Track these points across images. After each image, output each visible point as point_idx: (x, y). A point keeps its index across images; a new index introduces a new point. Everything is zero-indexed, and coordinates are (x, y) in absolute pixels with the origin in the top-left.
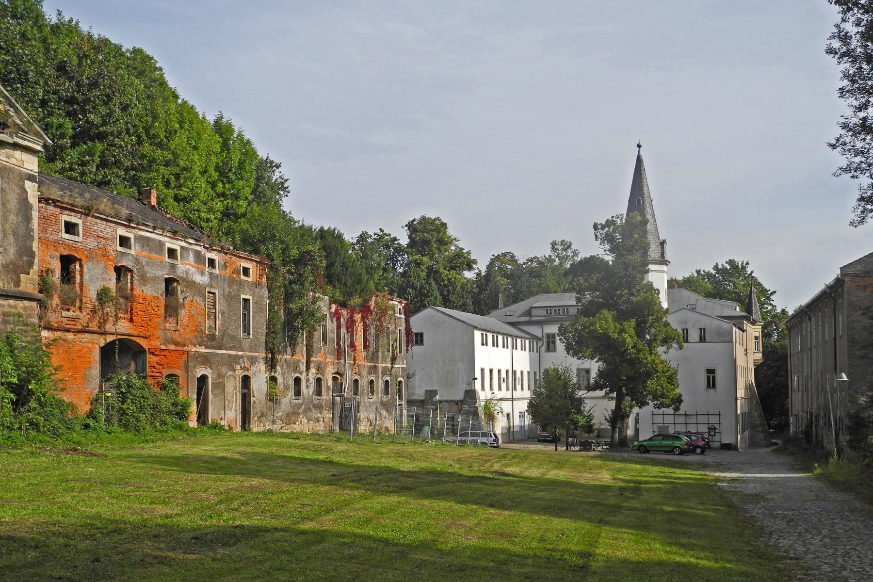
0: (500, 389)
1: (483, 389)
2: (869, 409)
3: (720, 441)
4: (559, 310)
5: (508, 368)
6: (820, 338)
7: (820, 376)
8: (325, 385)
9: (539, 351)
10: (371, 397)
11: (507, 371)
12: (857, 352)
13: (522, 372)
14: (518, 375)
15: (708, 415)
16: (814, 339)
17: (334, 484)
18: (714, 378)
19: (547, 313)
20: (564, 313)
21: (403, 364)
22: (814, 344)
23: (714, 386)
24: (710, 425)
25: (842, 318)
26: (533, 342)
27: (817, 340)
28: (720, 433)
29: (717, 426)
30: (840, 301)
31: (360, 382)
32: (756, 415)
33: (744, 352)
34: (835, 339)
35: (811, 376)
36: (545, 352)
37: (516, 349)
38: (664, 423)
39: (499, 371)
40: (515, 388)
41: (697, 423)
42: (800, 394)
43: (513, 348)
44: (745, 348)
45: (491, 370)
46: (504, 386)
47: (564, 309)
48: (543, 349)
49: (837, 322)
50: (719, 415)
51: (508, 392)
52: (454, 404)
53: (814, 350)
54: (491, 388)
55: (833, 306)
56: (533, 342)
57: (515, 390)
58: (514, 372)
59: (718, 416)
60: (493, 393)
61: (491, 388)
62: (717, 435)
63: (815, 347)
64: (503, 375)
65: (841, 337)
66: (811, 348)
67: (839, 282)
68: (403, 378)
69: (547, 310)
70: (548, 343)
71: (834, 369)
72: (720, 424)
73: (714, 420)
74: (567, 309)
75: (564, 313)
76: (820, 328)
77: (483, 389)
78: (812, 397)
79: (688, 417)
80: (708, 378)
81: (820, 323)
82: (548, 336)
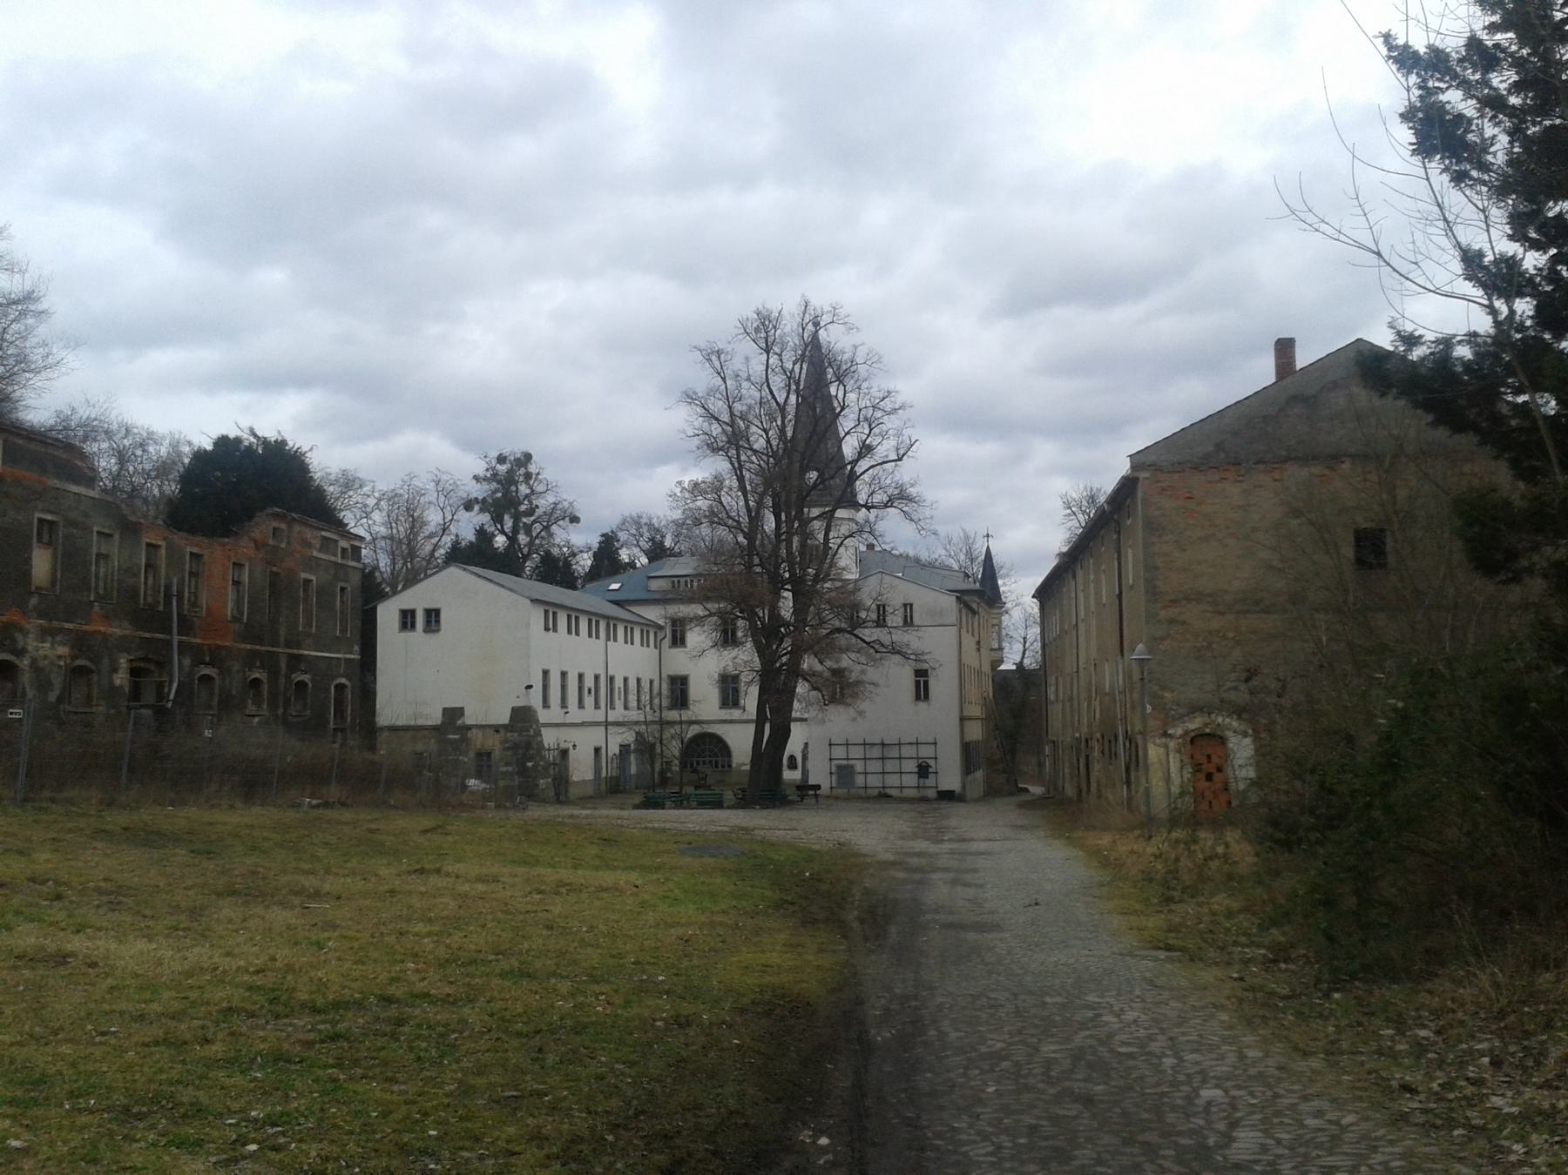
0: (581, 705)
1: (546, 704)
2: (1186, 718)
3: (937, 787)
4: (692, 581)
5: (597, 672)
6: (1092, 602)
7: (1092, 668)
11: (597, 677)
12: (1163, 613)
13: (626, 680)
14: (619, 683)
15: (917, 744)
16: (1082, 608)
18: (926, 683)
19: (673, 587)
20: (686, 585)
21: (351, 653)
22: (1082, 614)
23: (927, 697)
24: (920, 761)
25: (1134, 556)
26: (648, 632)
27: (1086, 608)
28: (936, 773)
29: (932, 762)
30: (1129, 522)
31: (217, 682)
32: (995, 746)
33: (974, 646)
34: (1120, 596)
35: (1077, 672)
36: (670, 647)
37: (615, 640)
38: (848, 759)
39: (581, 676)
41: (900, 758)
42: (1060, 706)
44: (977, 639)
45: (564, 674)
46: (589, 701)
47: (686, 582)
48: (667, 642)
49: (1123, 559)
50: (935, 744)
51: (598, 711)
52: (492, 732)
53: (1082, 628)
54: (564, 704)
55: (1115, 537)
56: (648, 632)
57: (613, 708)
60: (567, 713)
61: (564, 704)
62: (932, 778)
63: (1083, 620)
65: (1132, 588)
66: (1077, 624)
67: (1127, 487)
68: (347, 677)
70: (674, 633)
71: (1118, 652)
72: (936, 758)
73: (926, 752)
75: (686, 585)
76: (1092, 585)
77: (546, 704)
78: (1079, 703)
79: (886, 749)
80: (917, 683)
81: (1092, 577)
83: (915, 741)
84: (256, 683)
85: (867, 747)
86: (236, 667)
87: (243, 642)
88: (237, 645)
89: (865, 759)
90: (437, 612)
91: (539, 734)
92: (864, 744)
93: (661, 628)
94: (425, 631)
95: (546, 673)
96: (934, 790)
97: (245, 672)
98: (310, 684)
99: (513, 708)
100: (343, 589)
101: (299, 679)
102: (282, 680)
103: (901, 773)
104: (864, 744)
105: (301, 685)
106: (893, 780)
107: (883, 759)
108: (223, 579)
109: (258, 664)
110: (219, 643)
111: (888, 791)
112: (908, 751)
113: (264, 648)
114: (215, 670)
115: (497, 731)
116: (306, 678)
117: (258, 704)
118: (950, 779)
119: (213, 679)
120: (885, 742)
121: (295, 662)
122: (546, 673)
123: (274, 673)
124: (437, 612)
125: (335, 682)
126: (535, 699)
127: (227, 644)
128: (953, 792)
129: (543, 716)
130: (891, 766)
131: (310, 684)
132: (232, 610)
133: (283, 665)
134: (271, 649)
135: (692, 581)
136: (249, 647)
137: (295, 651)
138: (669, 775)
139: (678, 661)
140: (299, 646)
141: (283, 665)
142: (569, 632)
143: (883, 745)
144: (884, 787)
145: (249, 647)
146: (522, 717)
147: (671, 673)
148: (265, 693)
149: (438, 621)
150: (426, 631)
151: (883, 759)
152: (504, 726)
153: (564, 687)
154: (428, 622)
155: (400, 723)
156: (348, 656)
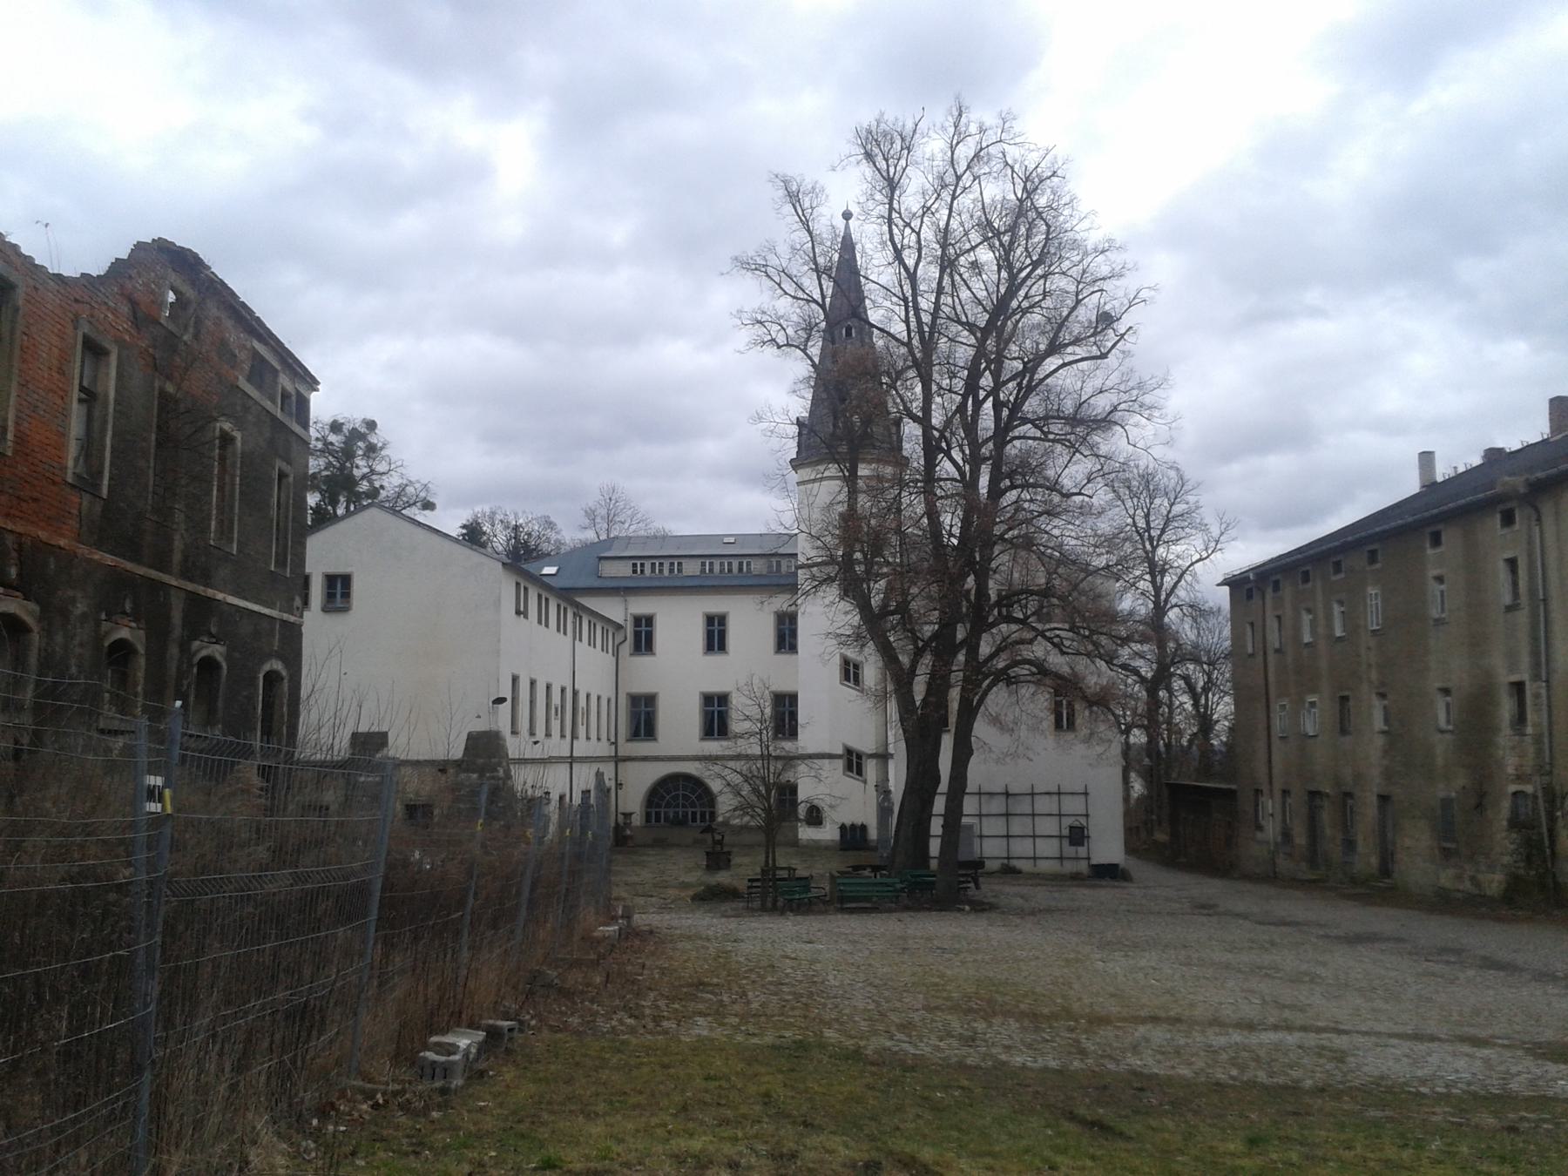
3: (1089, 859)
4: (661, 564)
5: (564, 685)
8: (1066, 633)
9: (616, 654)
10: (116, 725)
11: (563, 690)
13: (588, 696)
14: (582, 702)
15: (1059, 794)
17: (1536, 1043)
19: (635, 572)
31: (36, 637)
36: (631, 655)
37: (581, 640)
40: (574, 736)
43: (574, 639)
48: (627, 647)
50: (1086, 794)
58: (575, 693)
59: (1036, 797)
64: (556, 699)
69: (703, 564)
70: (637, 635)
73: (1072, 805)
74: (680, 564)
77: (514, 732)
79: (1011, 800)
82: (638, 620)
83: (1056, 790)
84: (122, 650)
85: (983, 797)
86: (80, 608)
87: (99, 545)
88: (83, 550)
89: (1033, 815)
90: (346, 580)
91: (508, 776)
92: (980, 794)
93: (619, 627)
94: (325, 610)
95: (515, 679)
96: (1086, 862)
97: (98, 623)
98: (224, 665)
99: (470, 736)
100: (282, 476)
101: (204, 653)
102: (174, 651)
103: (1034, 837)
104: (980, 794)
105: (209, 664)
106: (1021, 848)
107: (1007, 815)
108: (61, 372)
109: (128, 607)
110: (43, 535)
111: (1015, 863)
112: (1043, 804)
113: (141, 570)
114: (33, 606)
115: (443, 771)
116: (217, 651)
117: (123, 706)
118: (1108, 846)
119: (28, 630)
120: (1010, 792)
121: (201, 611)
122: (515, 679)
123: (158, 632)
124: (346, 580)
125: (267, 667)
126: (504, 726)
127: (62, 542)
128: (1116, 866)
129: (515, 747)
130: (1017, 827)
131: (224, 665)
132: (76, 460)
133: (177, 617)
134: (154, 574)
135: (661, 564)
136: (109, 559)
137: (200, 589)
138: (628, 832)
139: (644, 674)
140: (206, 579)
141: (177, 617)
142: (540, 622)
143: (1007, 794)
144: (1008, 858)
145: (109, 559)
146: (484, 747)
147: (629, 690)
148: (141, 675)
149: (347, 595)
150: (325, 610)
151: (1007, 815)
152: (458, 764)
153: (532, 702)
154: (330, 596)
155: (421, 758)
156: (286, 616)
